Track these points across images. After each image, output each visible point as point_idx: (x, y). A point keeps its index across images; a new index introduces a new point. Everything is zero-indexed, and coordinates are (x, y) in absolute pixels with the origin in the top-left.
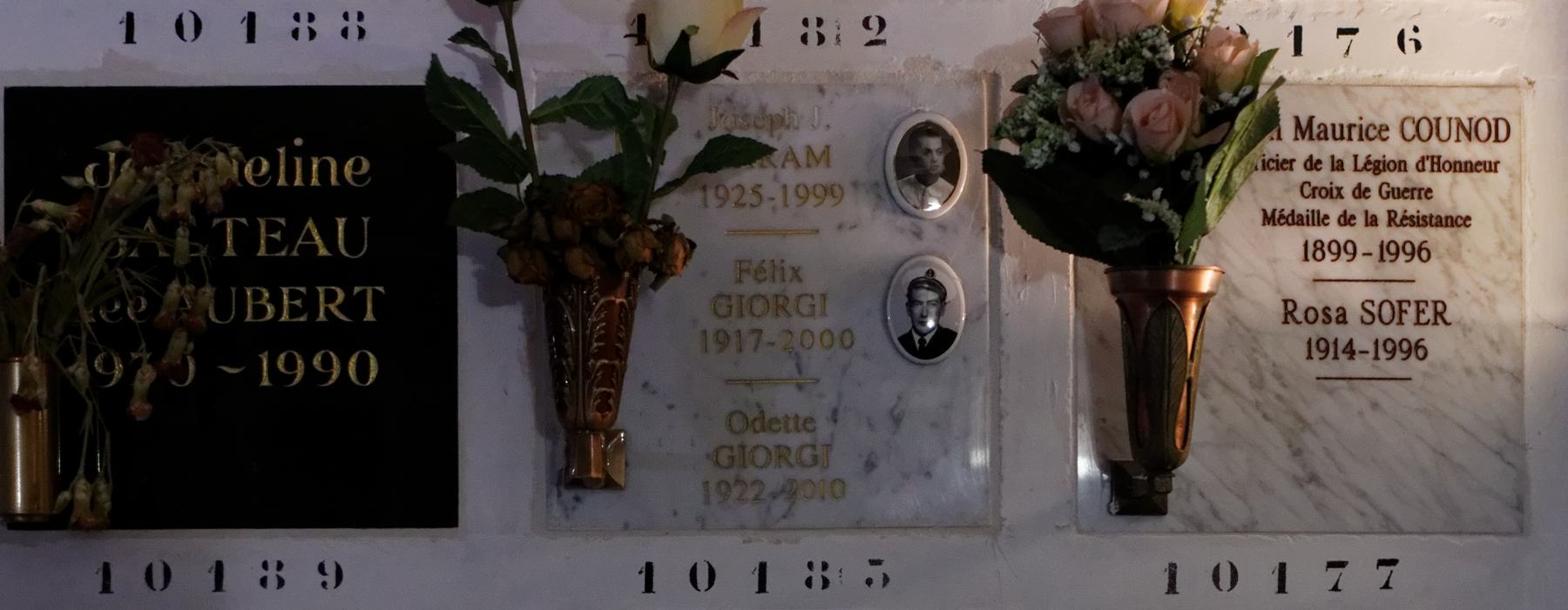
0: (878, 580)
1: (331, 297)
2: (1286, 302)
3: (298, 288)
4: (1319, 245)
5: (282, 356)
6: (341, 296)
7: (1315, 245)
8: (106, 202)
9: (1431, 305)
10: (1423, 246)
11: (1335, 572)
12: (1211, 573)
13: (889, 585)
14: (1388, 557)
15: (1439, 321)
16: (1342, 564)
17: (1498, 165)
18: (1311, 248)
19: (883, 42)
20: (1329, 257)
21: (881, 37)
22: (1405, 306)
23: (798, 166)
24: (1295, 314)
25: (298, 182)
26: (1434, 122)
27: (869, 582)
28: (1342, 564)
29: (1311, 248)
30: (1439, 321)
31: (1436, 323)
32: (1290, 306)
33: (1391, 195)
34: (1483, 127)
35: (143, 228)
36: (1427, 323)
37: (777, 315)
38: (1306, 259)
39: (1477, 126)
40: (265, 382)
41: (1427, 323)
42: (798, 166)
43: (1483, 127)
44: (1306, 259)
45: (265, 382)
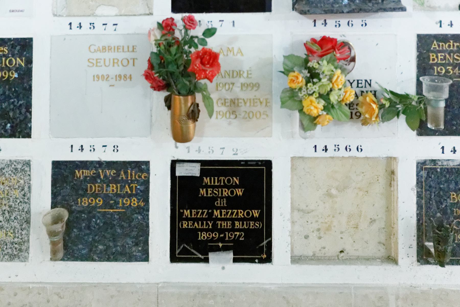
3: (187, 205)
17: (135, 60)
19: (237, 154)
21: (237, 153)
25: (212, 184)
28: (116, 25)
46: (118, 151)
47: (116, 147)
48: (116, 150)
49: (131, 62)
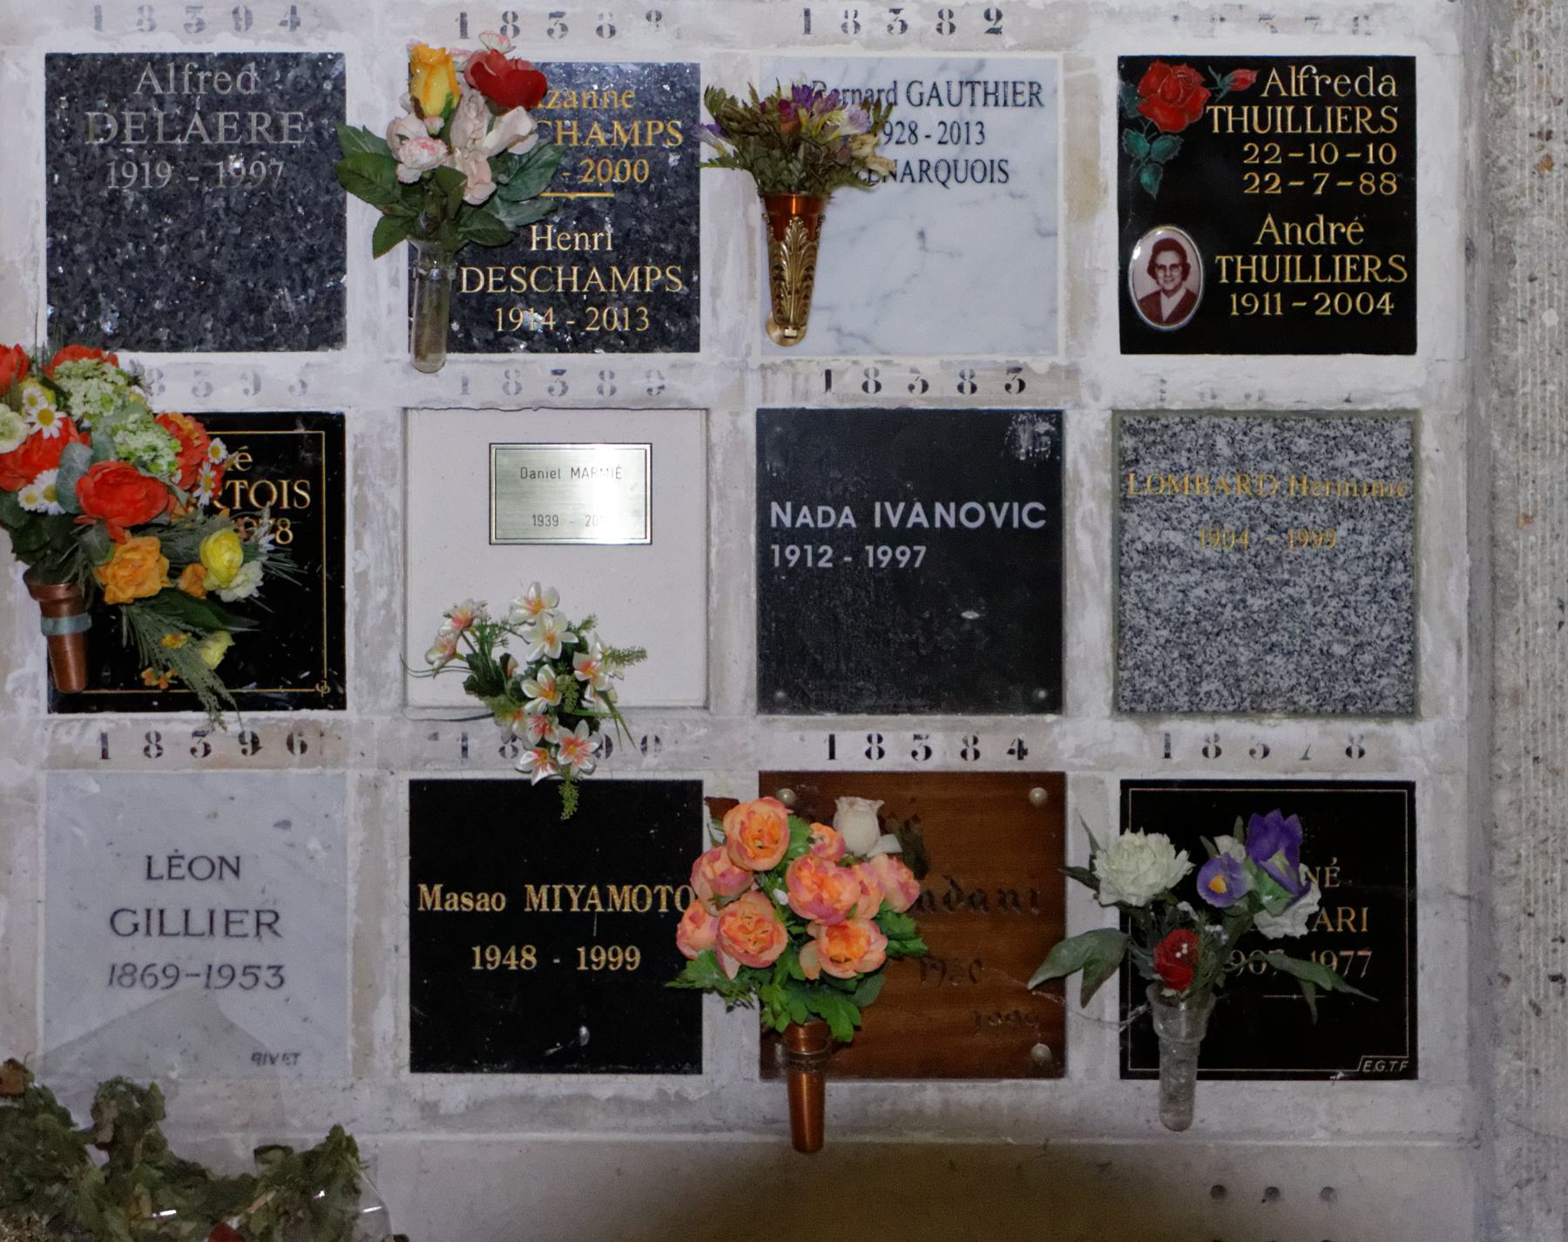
1: (1363, 114)
2: (921, 161)
5: (648, 908)
6: (1370, 115)
9: (1027, 86)
10: (226, 981)
12: (255, 21)
15: (1035, 101)
20: (157, 971)
22: (1020, 88)
26: (952, 164)
27: (193, 751)
30: (1035, 101)
31: (1031, 105)
32: (1035, 88)
34: (979, 175)
36: (1023, 105)
37: (238, 858)
39: (985, 174)
40: (1235, 313)
41: (1023, 105)
43: (979, 175)
45: (1235, 313)
46: (952, 28)
47: (946, 15)
48: (946, 28)
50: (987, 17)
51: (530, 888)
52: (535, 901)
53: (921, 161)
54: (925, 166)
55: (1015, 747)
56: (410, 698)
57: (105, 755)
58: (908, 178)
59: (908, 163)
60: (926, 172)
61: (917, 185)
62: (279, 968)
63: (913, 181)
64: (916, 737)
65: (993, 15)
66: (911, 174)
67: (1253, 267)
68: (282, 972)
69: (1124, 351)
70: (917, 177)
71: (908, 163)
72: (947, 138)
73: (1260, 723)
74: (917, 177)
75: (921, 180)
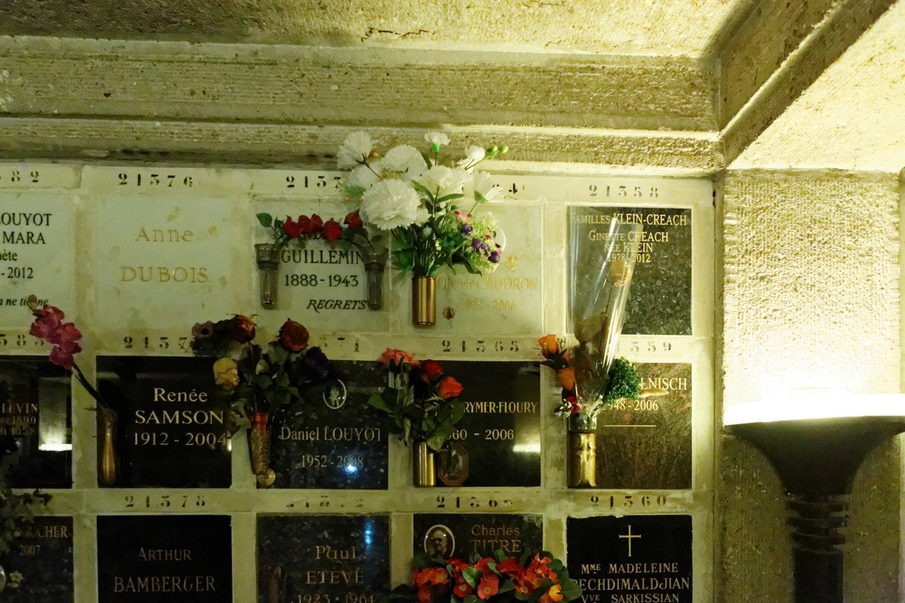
0: (322, 184)
2: (28, 233)
4: (295, 277)
7: (292, 277)
8: (493, 434)
11: (171, 179)
13: (327, 186)
14: (172, 175)
16: (173, 177)
17: (50, 217)
18: (290, 279)
23: (24, 215)
24: (33, 239)
27: (318, 184)
28: (173, 177)
29: (290, 279)
32: (30, 235)
33: (292, 258)
35: (68, 453)
36: (317, 262)
38: (287, 285)
42: (24, 215)
44: (287, 285)
47: (654, 189)
49: (45, 218)
50: (288, 180)
51: (583, 566)
52: (625, 585)
53: (28, 233)
54: (30, 235)
55: (512, 189)
56: (246, 435)
57: (148, 506)
58: (20, 241)
59: (41, 234)
60: (31, 238)
61: (26, 245)
62: (355, 276)
63: (23, 243)
64: (320, 177)
65: (290, 179)
66: (22, 239)
67: (604, 584)
68: (357, 279)
69: (227, 519)
70: (15, 241)
71: (41, 234)
72: (13, 274)
73: (218, 171)
74: (26, 241)
75: (28, 243)
